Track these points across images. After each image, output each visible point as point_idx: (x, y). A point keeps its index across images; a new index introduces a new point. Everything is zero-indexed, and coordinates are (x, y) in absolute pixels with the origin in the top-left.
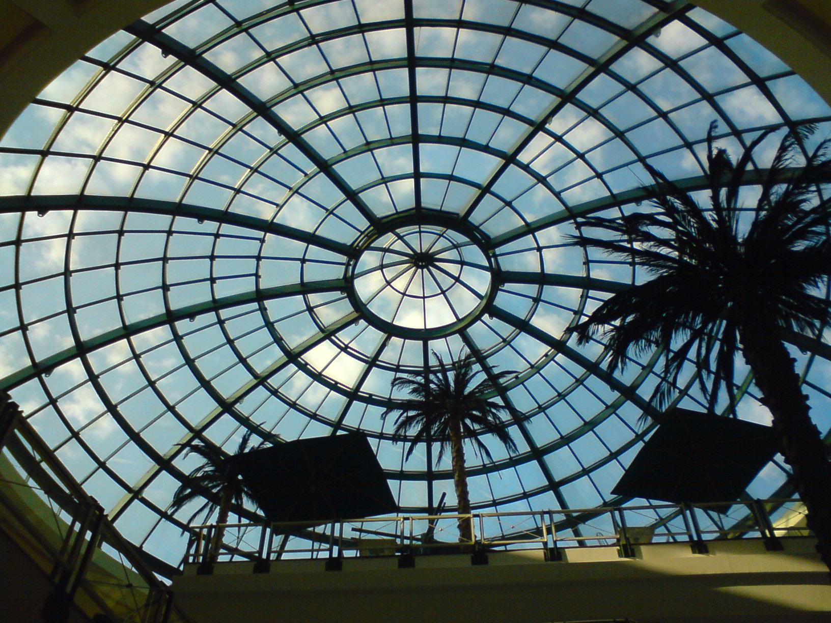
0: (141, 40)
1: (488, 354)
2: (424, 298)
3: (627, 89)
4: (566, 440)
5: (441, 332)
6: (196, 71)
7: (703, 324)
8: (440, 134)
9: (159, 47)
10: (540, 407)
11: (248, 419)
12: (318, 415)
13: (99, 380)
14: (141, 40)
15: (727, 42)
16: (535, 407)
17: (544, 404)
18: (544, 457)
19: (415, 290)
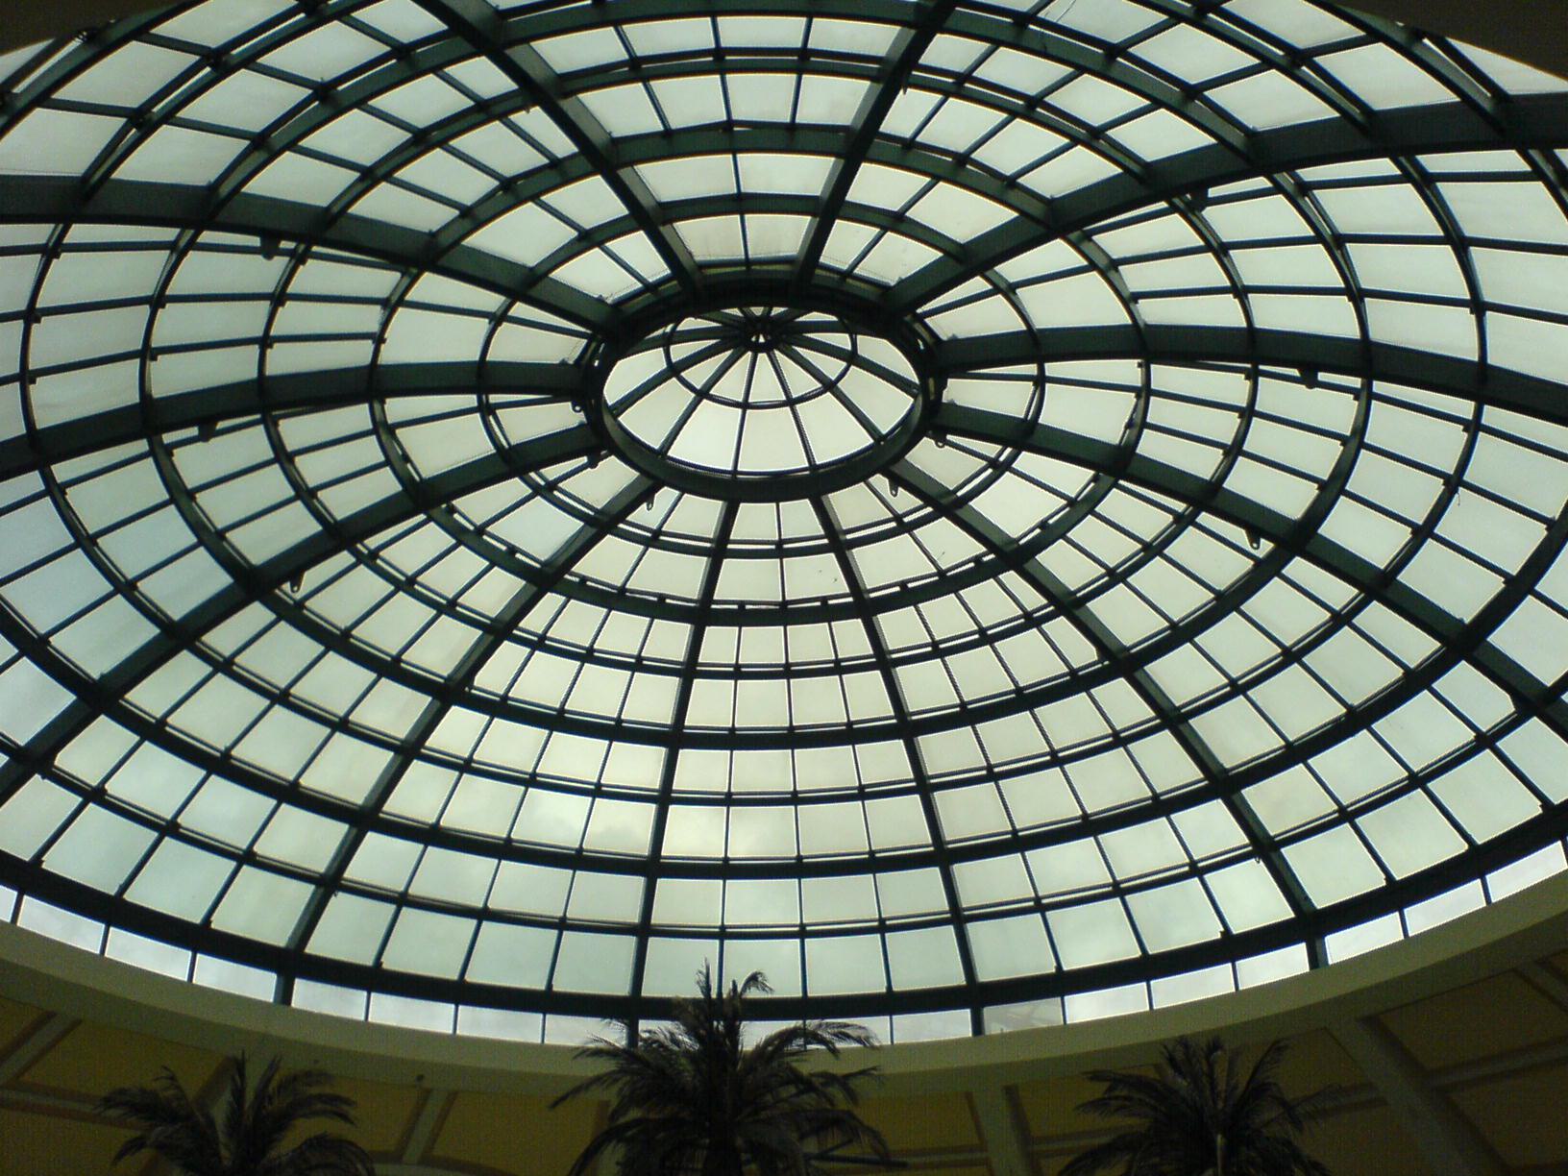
0: (61, 226)
1: (968, 493)
2: (745, 405)
3: (1016, 451)
4: (1296, 753)
5: (849, 471)
6: (829, 238)
7: (717, 545)
8: (550, 985)
9: (972, 277)
10: (1193, 864)
11: (295, 784)
12: (595, 651)
13: (44, 866)
14: (61, 226)
15: (1443, 187)
16: (1027, 896)
17: (1352, 804)
18: (919, 738)
19: (767, 387)
